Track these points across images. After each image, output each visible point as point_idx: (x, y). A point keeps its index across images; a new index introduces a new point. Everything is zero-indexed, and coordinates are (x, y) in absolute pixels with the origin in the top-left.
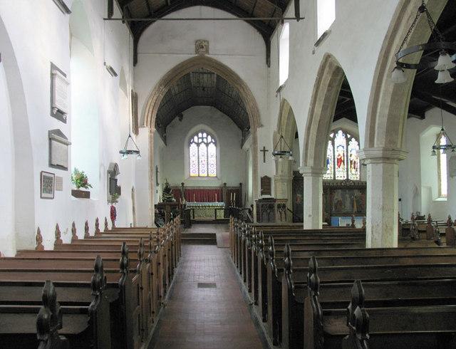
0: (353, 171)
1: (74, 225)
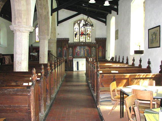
0: (88, 38)
1: (119, 56)
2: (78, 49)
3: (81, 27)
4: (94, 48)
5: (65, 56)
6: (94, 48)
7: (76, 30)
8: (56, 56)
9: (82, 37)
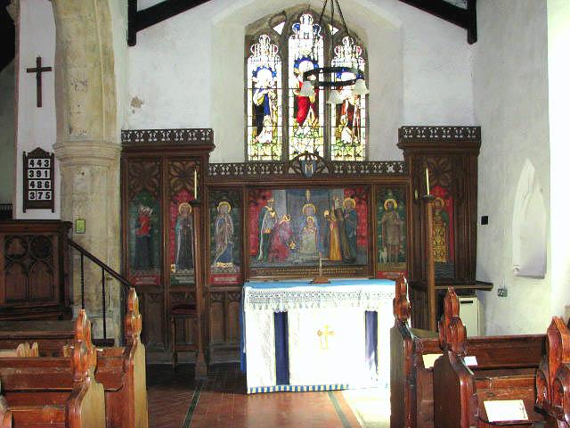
0: (346, 135)
2: (276, 213)
3: (297, 62)
4: (390, 201)
5: (186, 262)
6: (390, 201)
7: (264, 79)
8: (117, 270)
9: (300, 130)
